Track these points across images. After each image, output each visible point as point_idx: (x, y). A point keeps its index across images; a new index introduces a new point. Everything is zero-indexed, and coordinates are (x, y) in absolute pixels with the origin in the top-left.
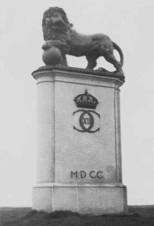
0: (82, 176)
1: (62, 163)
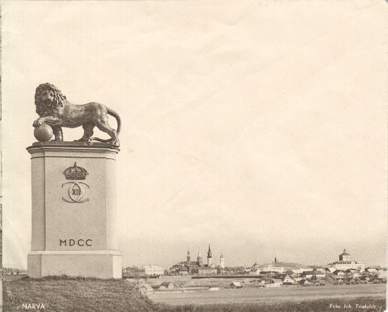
0: (71, 244)
1: (146, 307)
